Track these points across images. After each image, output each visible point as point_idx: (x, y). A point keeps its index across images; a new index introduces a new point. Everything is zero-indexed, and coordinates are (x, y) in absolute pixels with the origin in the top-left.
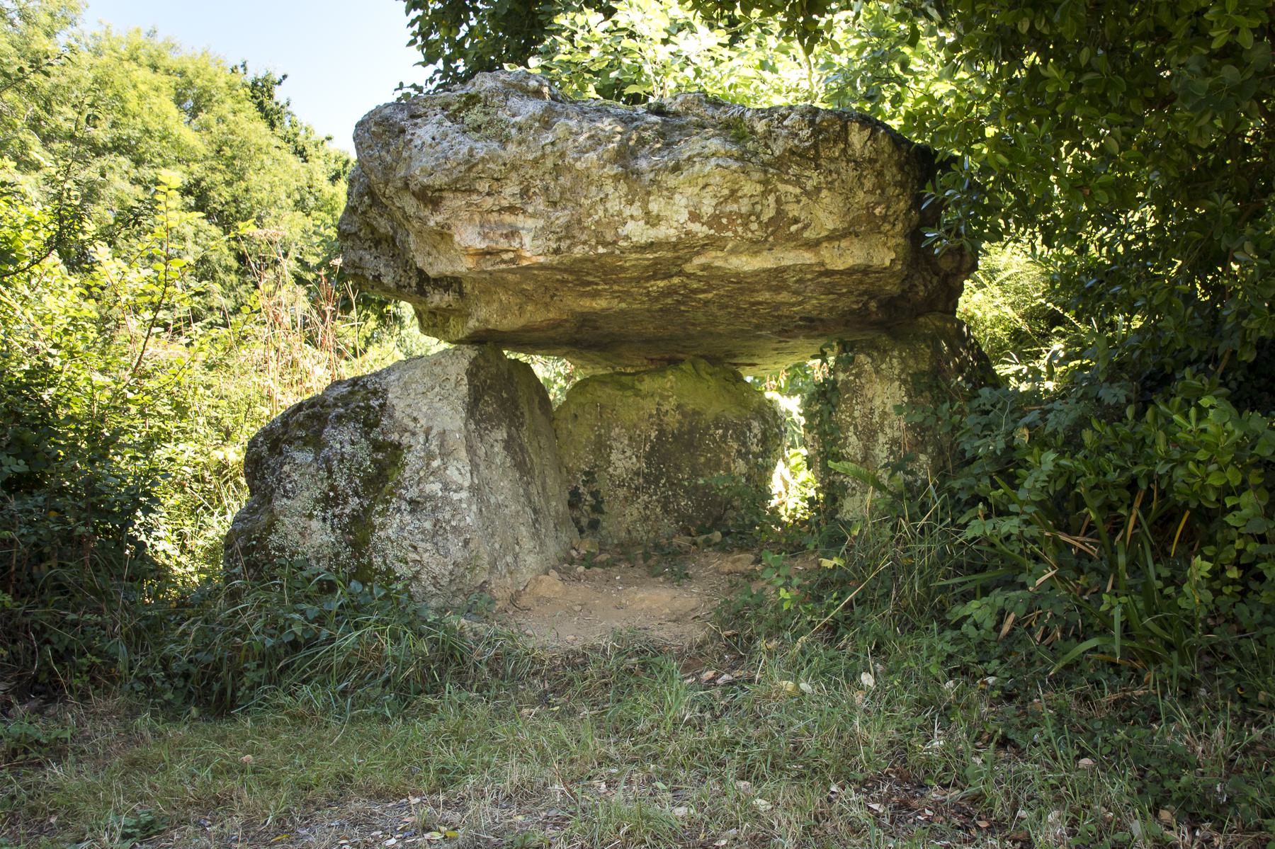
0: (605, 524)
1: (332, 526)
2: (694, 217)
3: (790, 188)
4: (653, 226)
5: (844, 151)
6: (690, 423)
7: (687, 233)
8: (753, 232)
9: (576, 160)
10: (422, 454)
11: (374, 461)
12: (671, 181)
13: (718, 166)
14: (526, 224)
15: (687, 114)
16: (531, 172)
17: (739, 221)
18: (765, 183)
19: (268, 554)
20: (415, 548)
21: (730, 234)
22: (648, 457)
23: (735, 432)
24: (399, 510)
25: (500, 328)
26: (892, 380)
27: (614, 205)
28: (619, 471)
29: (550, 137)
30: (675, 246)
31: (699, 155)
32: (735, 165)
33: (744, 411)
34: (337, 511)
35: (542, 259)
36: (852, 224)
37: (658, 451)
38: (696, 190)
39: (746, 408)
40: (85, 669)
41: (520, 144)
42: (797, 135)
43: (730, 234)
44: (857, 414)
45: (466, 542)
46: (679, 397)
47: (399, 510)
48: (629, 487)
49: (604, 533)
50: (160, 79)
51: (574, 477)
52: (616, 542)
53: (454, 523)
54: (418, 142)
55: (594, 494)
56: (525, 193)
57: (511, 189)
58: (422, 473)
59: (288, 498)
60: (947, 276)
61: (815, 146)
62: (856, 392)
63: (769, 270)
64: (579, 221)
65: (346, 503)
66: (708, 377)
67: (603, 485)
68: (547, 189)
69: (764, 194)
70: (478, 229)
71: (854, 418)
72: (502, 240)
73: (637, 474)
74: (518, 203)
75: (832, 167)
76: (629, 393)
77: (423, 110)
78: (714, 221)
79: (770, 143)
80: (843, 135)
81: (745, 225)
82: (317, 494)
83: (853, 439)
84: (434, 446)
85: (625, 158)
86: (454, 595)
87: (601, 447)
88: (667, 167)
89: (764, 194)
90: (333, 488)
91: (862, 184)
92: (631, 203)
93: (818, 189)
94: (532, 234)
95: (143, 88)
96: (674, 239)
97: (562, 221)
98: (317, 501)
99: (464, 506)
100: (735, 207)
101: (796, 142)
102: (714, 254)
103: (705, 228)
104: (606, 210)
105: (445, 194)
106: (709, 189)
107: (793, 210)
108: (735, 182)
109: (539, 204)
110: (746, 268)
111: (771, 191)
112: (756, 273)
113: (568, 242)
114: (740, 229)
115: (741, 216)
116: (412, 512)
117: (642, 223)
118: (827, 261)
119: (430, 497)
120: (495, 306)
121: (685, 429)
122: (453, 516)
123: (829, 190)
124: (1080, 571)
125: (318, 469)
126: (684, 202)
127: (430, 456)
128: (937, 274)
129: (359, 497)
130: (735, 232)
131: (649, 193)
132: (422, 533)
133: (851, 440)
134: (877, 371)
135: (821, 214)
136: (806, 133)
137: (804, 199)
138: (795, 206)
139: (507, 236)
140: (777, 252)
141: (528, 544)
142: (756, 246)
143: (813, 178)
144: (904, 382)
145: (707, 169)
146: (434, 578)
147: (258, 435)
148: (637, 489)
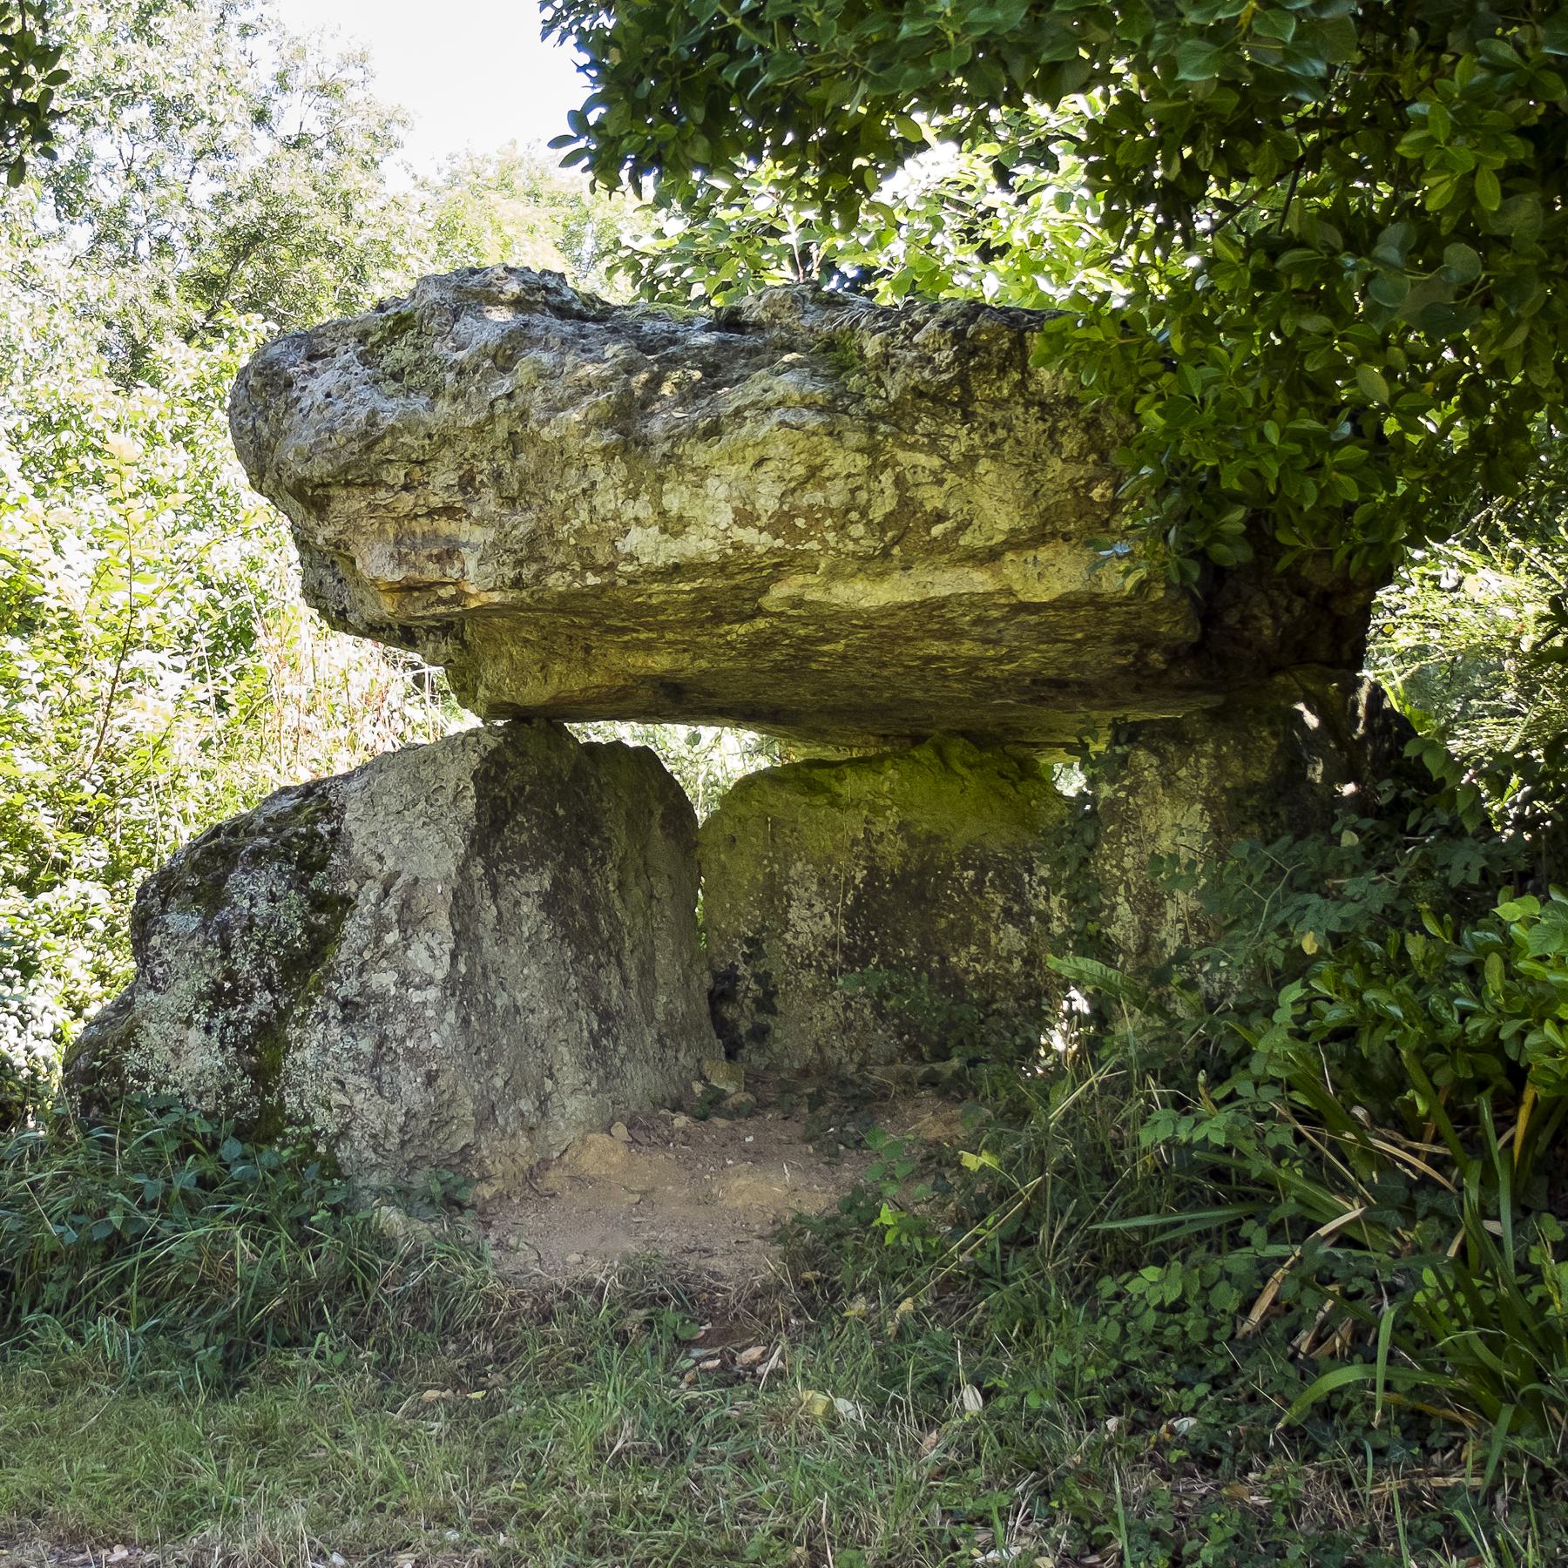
0: (778, 1034)
1: (222, 1042)
2: (744, 517)
3: (921, 459)
4: (675, 535)
5: (1021, 386)
6: (921, 856)
7: (737, 547)
8: (856, 541)
9: (543, 423)
10: (369, 921)
11: (310, 929)
12: (700, 454)
13: (782, 423)
14: (472, 534)
15: (773, 325)
16: (473, 446)
17: (828, 522)
18: (872, 450)
19: (121, 1084)
20: (342, 1084)
21: (814, 545)
22: (850, 916)
23: (999, 874)
24: (324, 1017)
25: (518, 701)
26: (1192, 800)
27: (607, 500)
28: (801, 940)
29: (507, 384)
30: (722, 568)
31: (754, 404)
32: (813, 421)
33: (1026, 835)
34: (234, 1014)
35: (496, 597)
36: (1046, 517)
37: (867, 905)
38: (745, 469)
39: (1032, 828)
40: (1403, 987)
41: (455, 399)
42: (930, 360)
43: (814, 545)
44: (1128, 863)
45: (431, 1078)
46: (902, 808)
47: (324, 1017)
48: (819, 968)
49: (777, 1048)
50: (539, 215)
51: (729, 947)
52: (796, 1065)
53: (410, 1044)
54: (305, 403)
55: (763, 979)
56: (467, 483)
57: (444, 476)
58: (367, 955)
59: (158, 990)
60: (1326, 597)
61: (962, 380)
62: (1127, 819)
63: (911, 605)
64: (551, 531)
65: (249, 1000)
66: (964, 771)
67: (778, 963)
68: (500, 476)
69: (873, 471)
70: (390, 549)
71: (1125, 871)
72: (431, 566)
73: (831, 945)
74: (457, 500)
75: (997, 416)
76: (821, 800)
77: (330, 345)
78: (782, 523)
79: (884, 377)
80: (1017, 355)
81: (841, 528)
82: (203, 985)
83: (1124, 910)
84: (389, 910)
85: (629, 416)
86: (412, 1167)
87: (774, 895)
88: (694, 429)
89: (873, 471)
90: (230, 975)
91: (1057, 447)
92: (634, 495)
93: (971, 459)
94: (478, 554)
95: (509, 230)
96: (715, 558)
97: (523, 530)
98: (201, 996)
99: (430, 1013)
100: (818, 497)
101: (927, 374)
102: (800, 579)
103: (766, 537)
104: (593, 510)
105: (333, 491)
106: (770, 466)
107: (932, 498)
108: (814, 452)
109: (489, 501)
110: (864, 604)
111: (885, 465)
112: (887, 611)
113: (534, 567)
114: (831, 537)
115: (831, 512)
116: (344, 1021)
117: (654, 530)
118: (1017, 587)
119: (380, 997)
120: (504, 663)
121: (913, 866)
122: (410, 1030)
123: (994, 458)
124: (1409, 1213)
125: (206, 943)
126: (722, 492)
127: (382, 926)
128: (1302, 593)
129: (272, 992)
130: (823, 541)
131: (661, 479)
132: (355, 1058)
133: (1120, 910)
134: (1168, 782)
135: (985, 503)
136: (945, 356)
137: (950, 477)
138: (935, 491)
139: (438, 559)
140: (919, 573)
141: (570, 1075)
142: (874, 564)
143: (960, 439)
144: (1210, 804)
145: (763, 431)
146: (374, 1136)
147: (151, 879)
148: (832, 972)
